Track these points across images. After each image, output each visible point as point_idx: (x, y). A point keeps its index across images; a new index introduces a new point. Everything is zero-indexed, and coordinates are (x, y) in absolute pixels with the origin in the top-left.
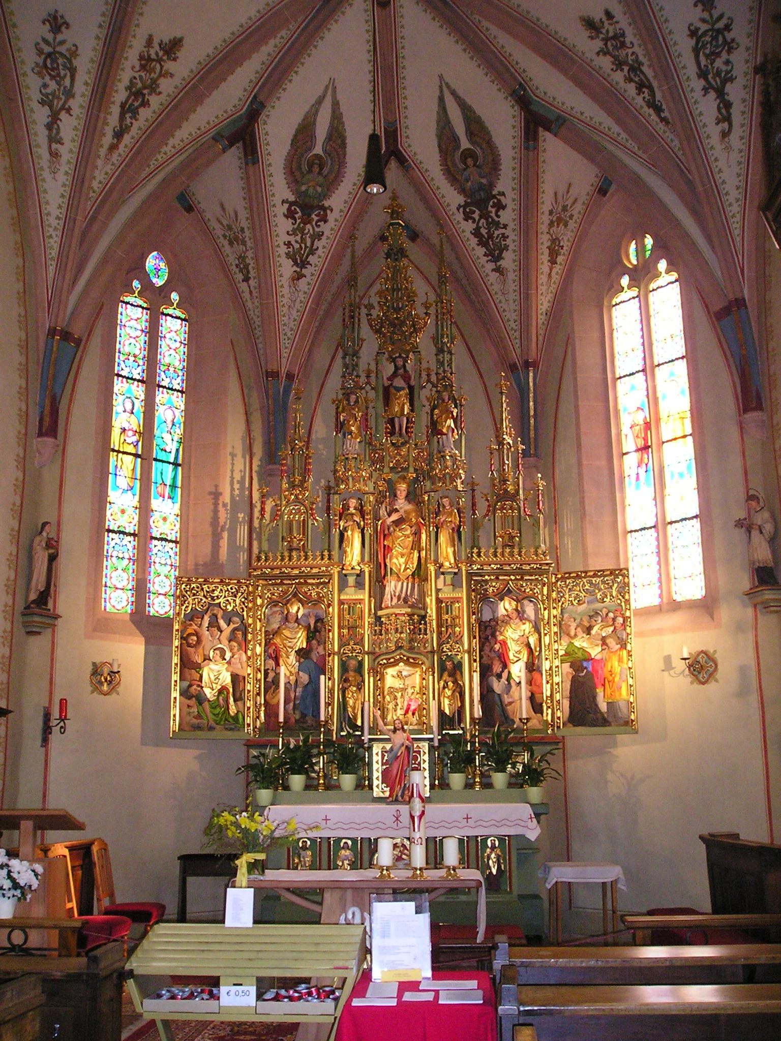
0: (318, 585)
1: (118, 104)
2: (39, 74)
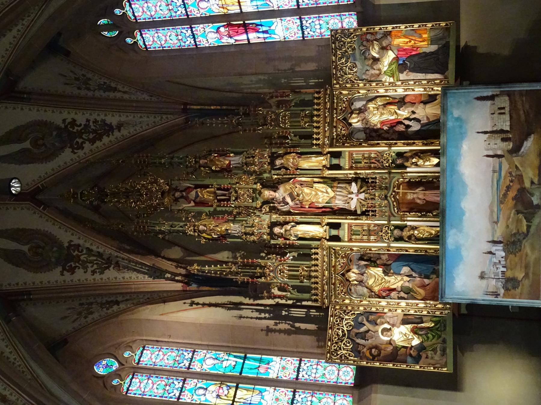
0: (336, 258)
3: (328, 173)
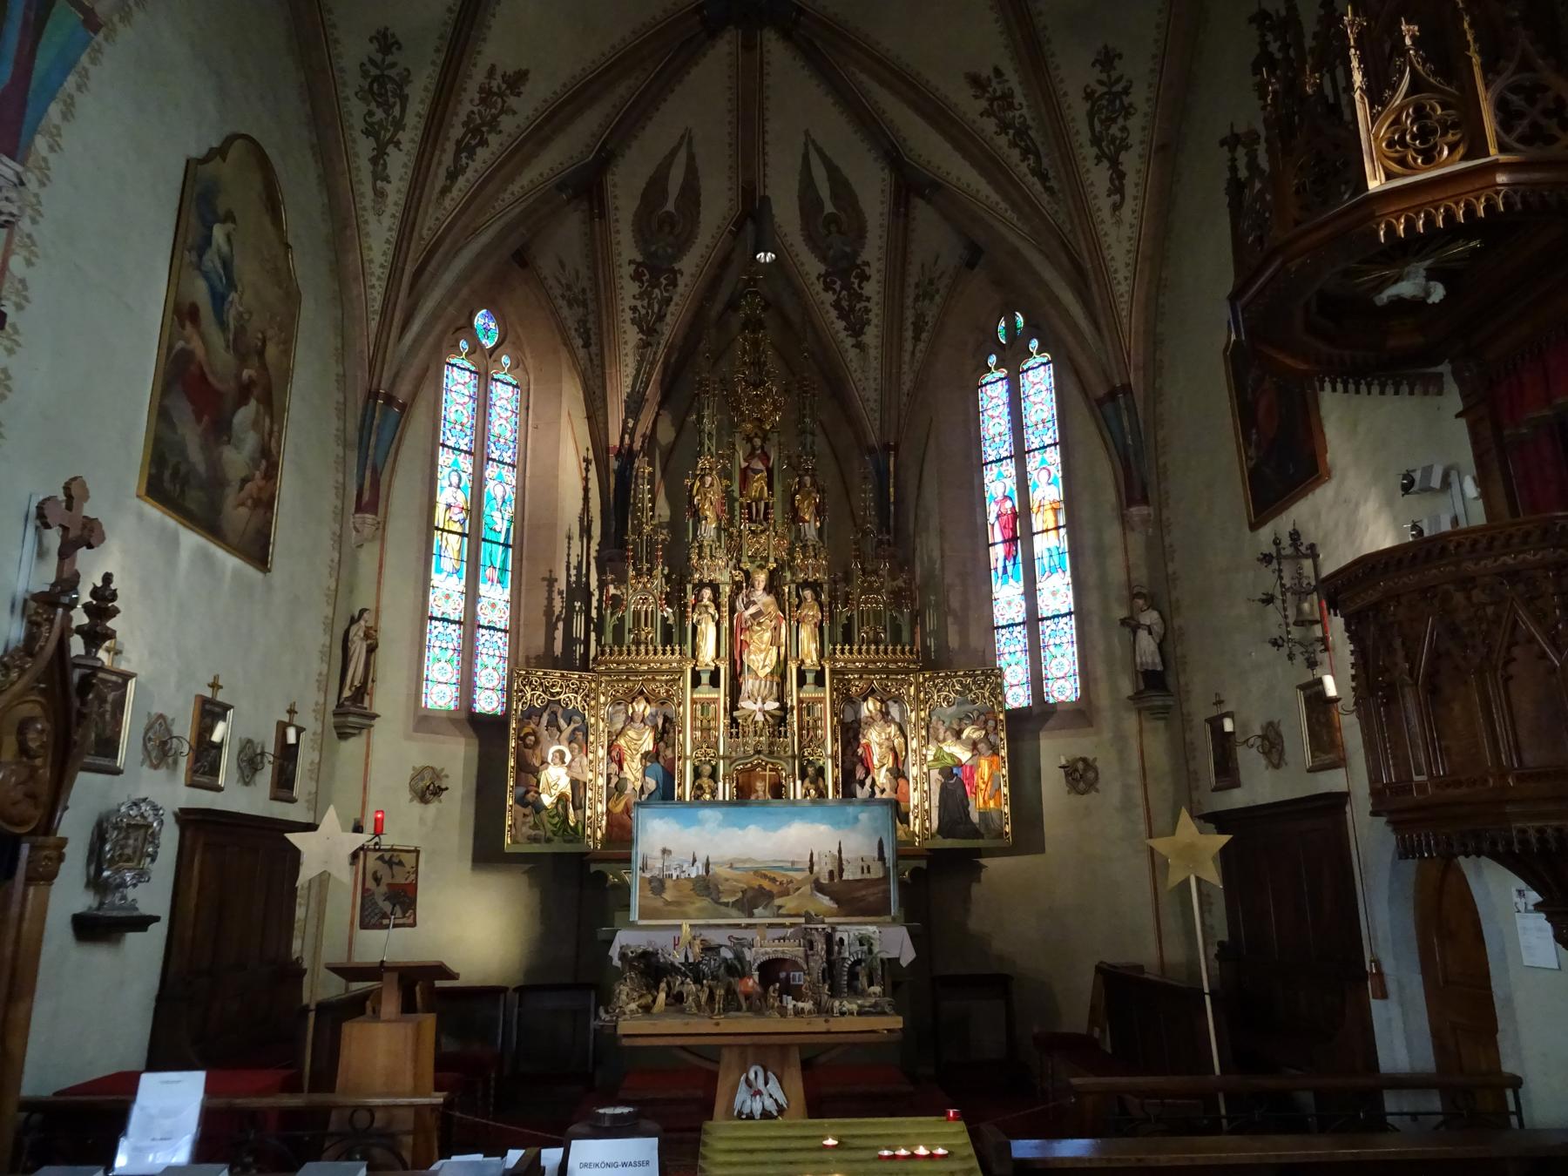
0: (667, 682)
2: (363, 99)
3: (793, 667)
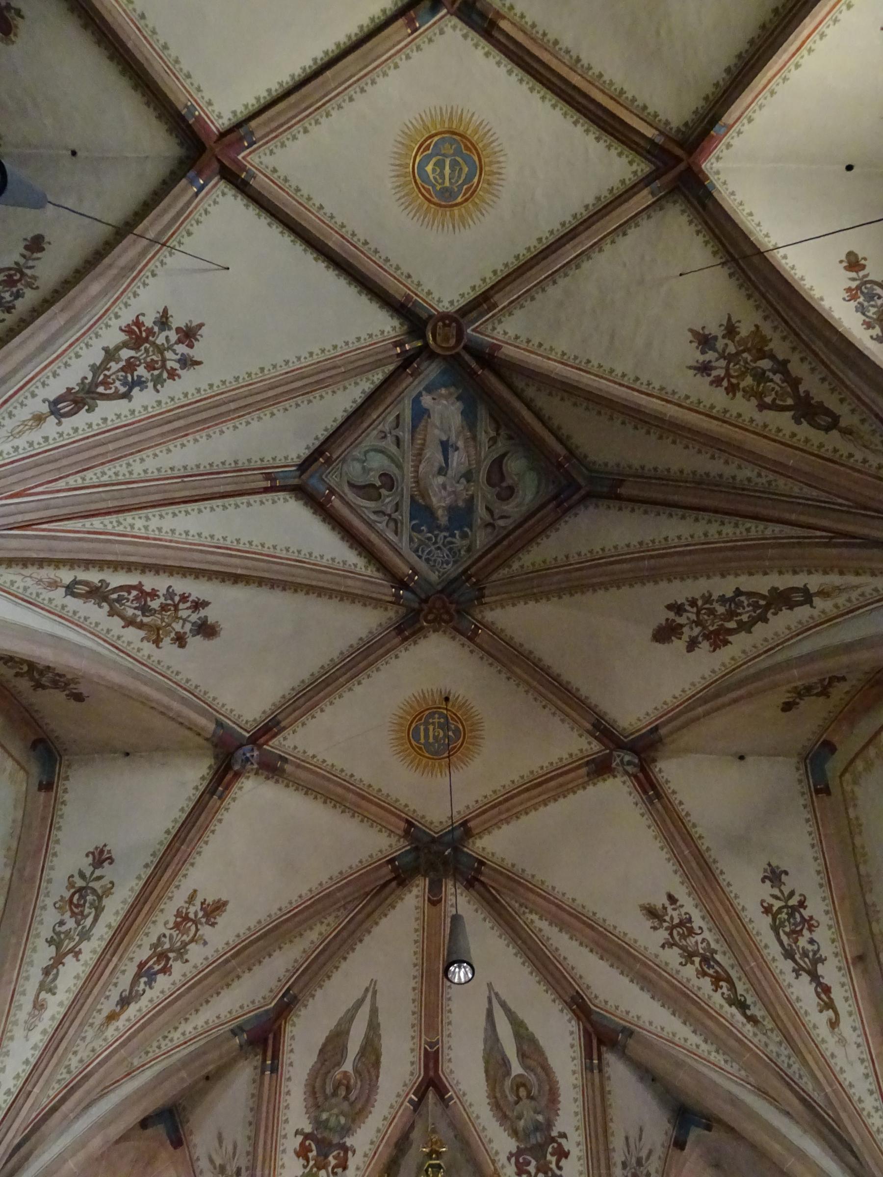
1: (137, 961)
